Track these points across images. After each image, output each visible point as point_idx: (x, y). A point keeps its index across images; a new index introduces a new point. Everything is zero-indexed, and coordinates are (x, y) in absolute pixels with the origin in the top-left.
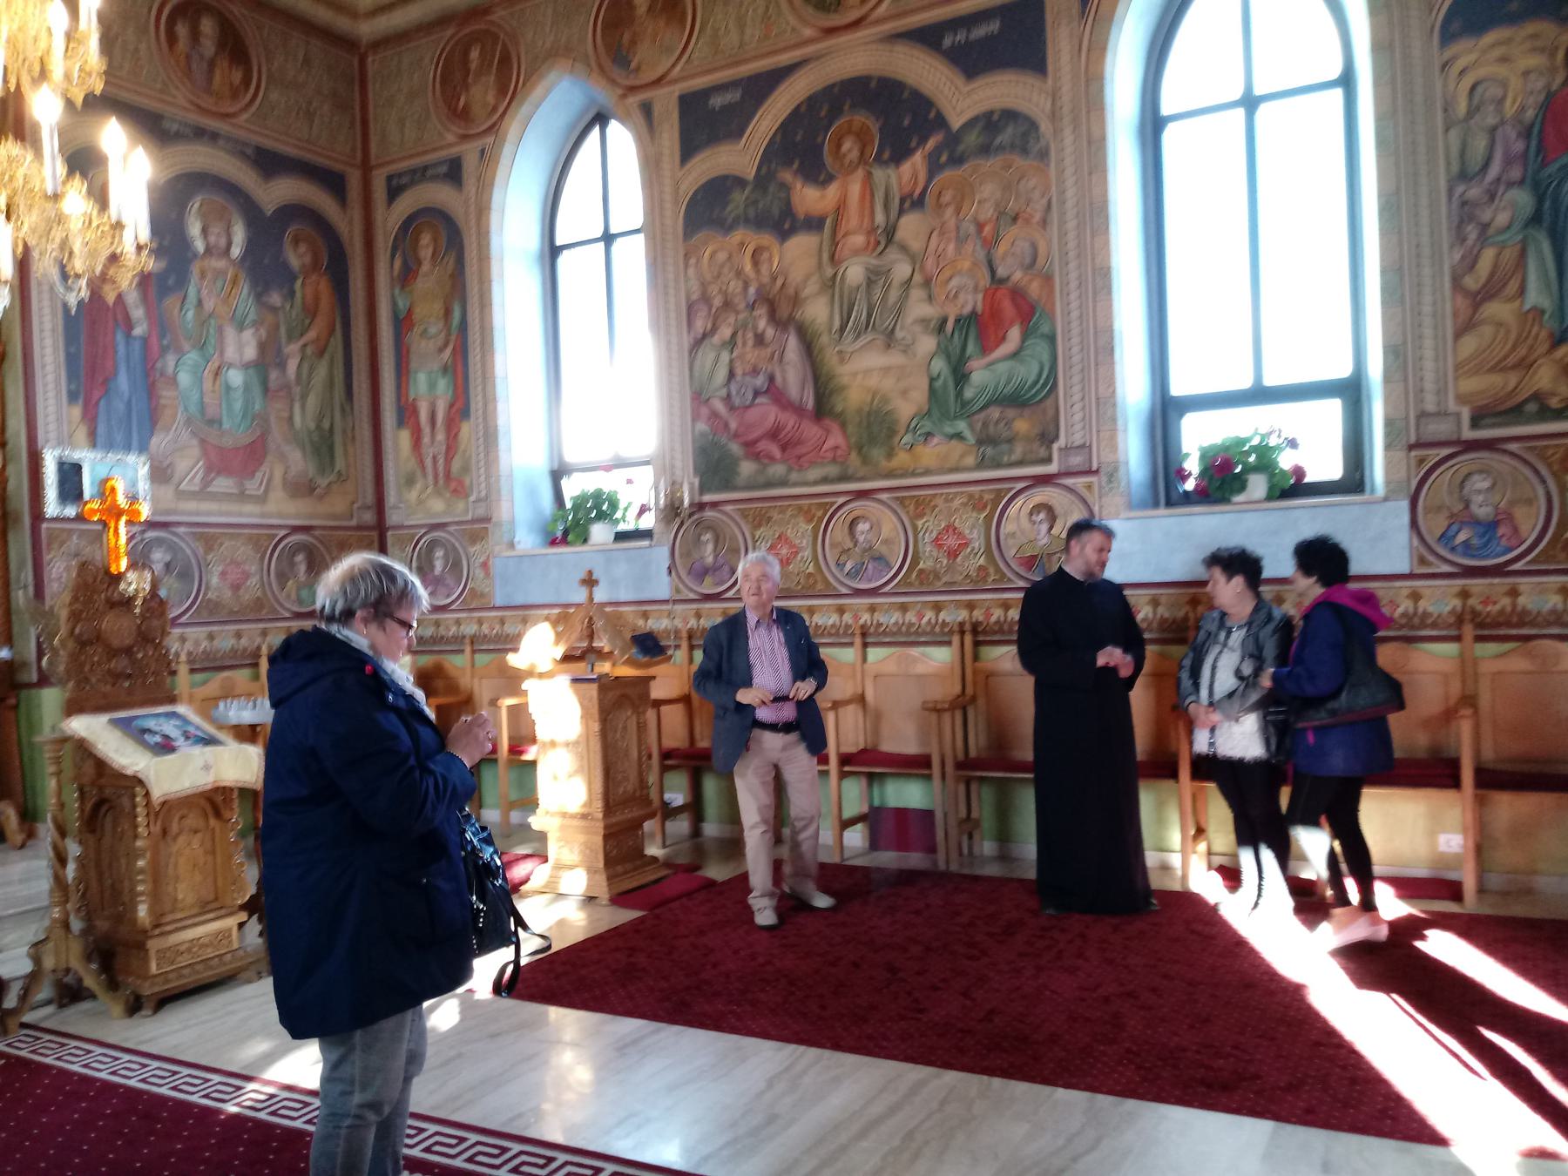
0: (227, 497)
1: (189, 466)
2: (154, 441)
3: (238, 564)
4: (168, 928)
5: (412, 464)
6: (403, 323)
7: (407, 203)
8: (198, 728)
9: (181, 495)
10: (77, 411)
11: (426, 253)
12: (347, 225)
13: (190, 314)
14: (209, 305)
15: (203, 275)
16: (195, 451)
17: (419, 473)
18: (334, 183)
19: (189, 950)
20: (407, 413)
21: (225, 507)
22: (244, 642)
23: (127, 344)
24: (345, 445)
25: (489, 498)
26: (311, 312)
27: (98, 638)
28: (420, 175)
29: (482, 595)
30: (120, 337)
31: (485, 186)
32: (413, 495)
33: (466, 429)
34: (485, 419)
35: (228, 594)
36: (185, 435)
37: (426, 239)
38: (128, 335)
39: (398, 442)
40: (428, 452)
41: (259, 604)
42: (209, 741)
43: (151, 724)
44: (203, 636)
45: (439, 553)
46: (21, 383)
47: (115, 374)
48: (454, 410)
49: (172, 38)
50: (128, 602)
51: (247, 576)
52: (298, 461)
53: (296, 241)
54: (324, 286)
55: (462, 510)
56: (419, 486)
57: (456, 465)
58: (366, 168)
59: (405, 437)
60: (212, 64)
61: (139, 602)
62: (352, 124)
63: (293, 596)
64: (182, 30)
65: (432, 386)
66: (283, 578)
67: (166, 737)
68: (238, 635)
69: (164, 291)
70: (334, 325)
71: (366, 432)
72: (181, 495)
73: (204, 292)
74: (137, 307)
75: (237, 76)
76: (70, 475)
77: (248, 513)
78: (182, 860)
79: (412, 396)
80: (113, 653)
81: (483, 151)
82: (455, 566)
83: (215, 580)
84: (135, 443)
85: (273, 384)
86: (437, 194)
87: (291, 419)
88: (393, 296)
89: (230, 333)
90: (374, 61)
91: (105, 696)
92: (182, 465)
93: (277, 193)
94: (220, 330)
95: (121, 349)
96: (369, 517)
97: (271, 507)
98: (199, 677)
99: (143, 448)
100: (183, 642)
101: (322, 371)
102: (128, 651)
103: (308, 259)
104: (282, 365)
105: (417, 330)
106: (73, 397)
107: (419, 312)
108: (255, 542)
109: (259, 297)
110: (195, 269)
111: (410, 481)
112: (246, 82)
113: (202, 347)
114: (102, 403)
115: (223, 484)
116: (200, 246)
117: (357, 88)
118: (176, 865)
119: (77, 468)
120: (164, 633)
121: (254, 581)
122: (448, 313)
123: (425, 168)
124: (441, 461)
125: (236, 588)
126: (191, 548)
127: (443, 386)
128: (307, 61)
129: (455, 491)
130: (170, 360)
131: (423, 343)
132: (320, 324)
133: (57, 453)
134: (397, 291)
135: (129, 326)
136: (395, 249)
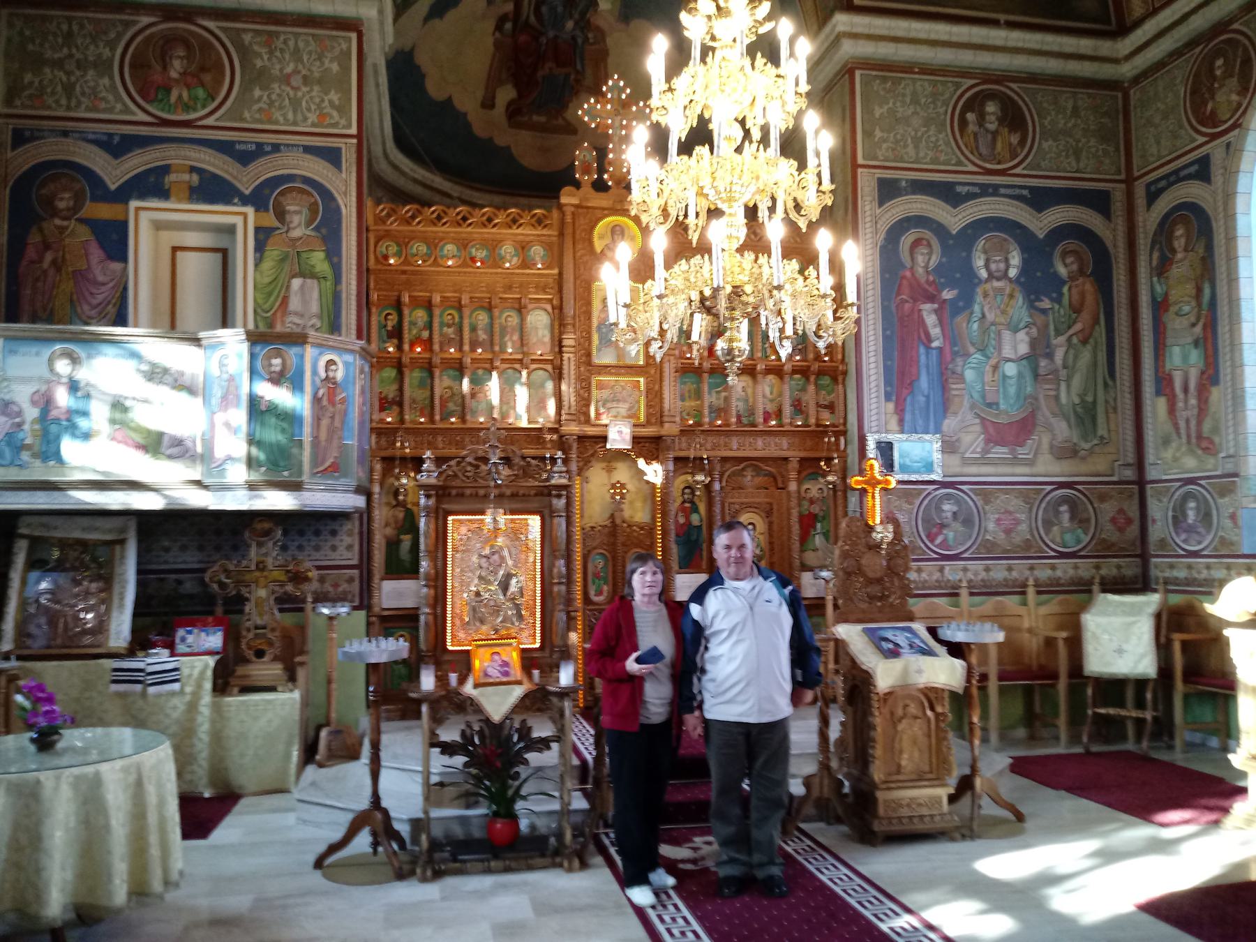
0: (1002, 462)
1: (973, 441)
2: (946, 422)
3: (1010, 513)
4: (893, 785)
5: (1168, 427)
6: (1160, 306)
7: (1164, 204)
8: (923, 641)
10: (891, 406)
11: (1179, 244)
12: (1110, 232)
13: (975, 326)
14: (990, 316)
15: (986, 295)
16: (978, 428)
17: (1174, 436)
18: (1099, 202)
19: (908, 805)
20: (1164, 384)
22: (1015, 574)
23: (927, 354)
24: (1107, 412)
25: (1236, 456)
26: (1077, 309)
27: (860, 571)
28: (1175, 178)
29: (1232, 544)
30: (922, 350)
31: (1231, 174)
32: (1168, 454)
33: (1215, 393)
34: (1234, 385)
35: (1002, 536)
36: (970, 418)
37: (1179, 232)
38: (928, 348)
39: (1156, 408)
40: (1182, 415)
41: (1028, 545)
42: (928, 652)
43: (889, 635)
44: (981, 567)
45: (1192, 504)
47: (918, 378)
49: (963, 123)
50: (876, 547)
51: (1018, 522)
52: (1063, 430)
53: (1064, 254)
55: (1213, 466)
56: (1174, 445)
57: (1207, 427)
58: (1130, 181)
59: (1162, 403)
60: (995, 134)
61: (884, 546)
62: (1117, 150)
63: (1058, 539)
64: (970, 116)
65: (1185, 358)
66: (1048, 524)
67: (897, 645)
68: (1010, 569)
71: (1127, 400)
72: (966, 462)
73: (986, 310)
74: (935, 326)
75: (1015, 139)
76: (886, 450)
77: (1020, 473)
78: (905, 737)
79: (1168, 366)
80: (870, 582)
81: (1228, 145)
82: (1206, 517)
83: (991, 526)
84: (932, 426)
85: (1042, 371)
86: (1191, 191)
87: (1057, 398)
89: (1007, 335)
91: (864, 611)
92: (967, 439)
93: (1041, 223)
94: (999, 334)
95: (923, 358)
96: (1129, 474)
97: (1040, 468)
98: (977, 599)
99: (938, 430)
100: (920, 573)
101: (1086, 355)
102: (879, 581)
103: (1075, 267)
104: (1050, 356)
105: (1173, 309)
106: (888, 398)
107: (1174, 295)
108: (1027, 498)
109: (1031, 306)
110: (979, 290)
111: (1166, 442)
112: (1022, 142)
113: (982, 350)
114: (909, 399)
115: (1000, 452)
116: (984, 274)
117: (1121, 117)
118: (901, 740)
119: (890, 446)
120: (907, 569)
121: (1023, 527)
122: (1199, 290)
123: (1176, 172)
124: (1193, 423)
125: (1008, 532)
126: (971, 501)
127: (1195, 356)
128: (1075, 110)
129: (1206, 450)
131: (1178, 320)
132: (1086, 316)
133: (876, 436)
134: (1155, 279)
135: (929, 339)
136: (1154, 243)
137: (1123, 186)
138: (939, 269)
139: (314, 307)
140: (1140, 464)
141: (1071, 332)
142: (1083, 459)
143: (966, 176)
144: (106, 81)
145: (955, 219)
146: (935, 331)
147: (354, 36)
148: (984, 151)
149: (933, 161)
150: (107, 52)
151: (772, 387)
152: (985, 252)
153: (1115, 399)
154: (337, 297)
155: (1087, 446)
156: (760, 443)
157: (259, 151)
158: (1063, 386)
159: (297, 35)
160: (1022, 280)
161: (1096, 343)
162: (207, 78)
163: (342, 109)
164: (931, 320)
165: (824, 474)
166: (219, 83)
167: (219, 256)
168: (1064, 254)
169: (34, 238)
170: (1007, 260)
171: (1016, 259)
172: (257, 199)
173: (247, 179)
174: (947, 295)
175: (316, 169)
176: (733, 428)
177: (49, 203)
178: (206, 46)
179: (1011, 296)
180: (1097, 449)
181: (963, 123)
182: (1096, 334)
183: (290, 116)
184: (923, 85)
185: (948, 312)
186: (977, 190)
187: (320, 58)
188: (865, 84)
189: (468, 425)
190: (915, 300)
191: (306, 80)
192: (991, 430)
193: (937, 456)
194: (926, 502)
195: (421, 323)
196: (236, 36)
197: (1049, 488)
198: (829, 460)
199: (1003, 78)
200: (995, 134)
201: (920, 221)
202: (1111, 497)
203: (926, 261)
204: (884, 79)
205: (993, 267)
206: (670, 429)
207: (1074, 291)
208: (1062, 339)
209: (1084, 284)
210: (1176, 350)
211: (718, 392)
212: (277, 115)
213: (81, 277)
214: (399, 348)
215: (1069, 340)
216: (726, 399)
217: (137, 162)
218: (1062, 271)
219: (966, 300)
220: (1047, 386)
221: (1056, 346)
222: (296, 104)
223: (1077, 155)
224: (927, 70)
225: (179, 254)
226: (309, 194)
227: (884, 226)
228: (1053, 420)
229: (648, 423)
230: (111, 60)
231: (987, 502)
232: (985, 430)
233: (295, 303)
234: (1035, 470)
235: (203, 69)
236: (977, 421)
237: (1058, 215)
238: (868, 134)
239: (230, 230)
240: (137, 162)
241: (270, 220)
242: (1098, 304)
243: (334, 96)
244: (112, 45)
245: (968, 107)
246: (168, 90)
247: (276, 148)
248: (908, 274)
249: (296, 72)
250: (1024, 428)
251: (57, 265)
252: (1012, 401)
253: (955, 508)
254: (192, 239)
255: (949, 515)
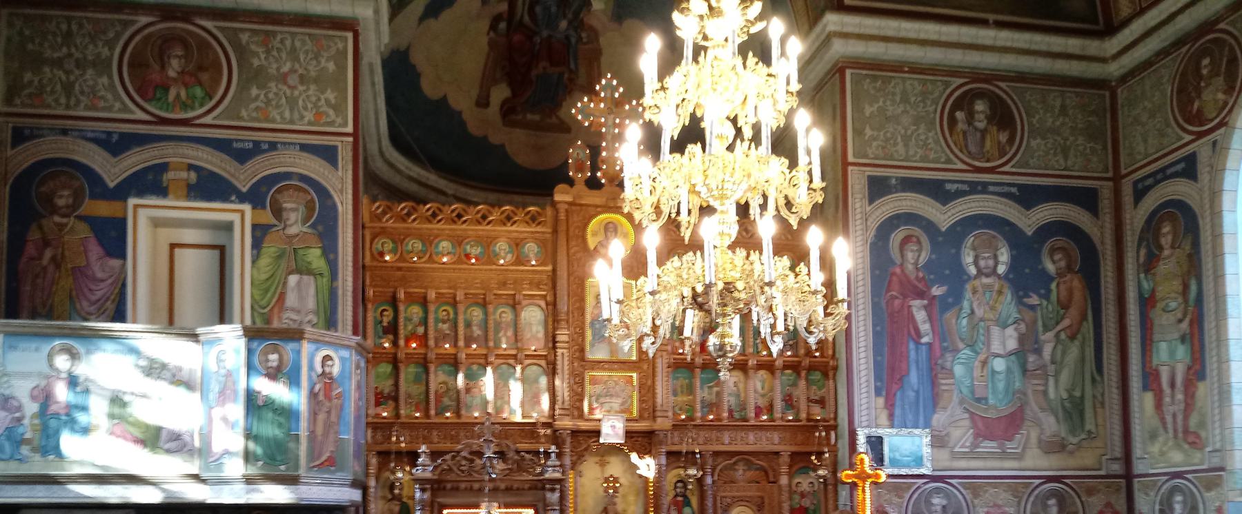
1: (962, 435)
2: (936, 417)
3: (999, 506)
5: (1156, 422)
6: (1147, 302)
7: (1151, 201)
9: (955, 456)
10: (881, 401)
11: (1166, 241)
12: (1098, 229)
13: (964, 322)
14: (979, 313)
15: (975, 292)
16: (967, 423)
17: (1161, 430)
18: (1087, 199)
20: (1151, 379)
21: (990, 464)
23: (917, 350)
25: (1223, 450)
26: (1065, 305)
28: (1162, 176)
30: (912, 346)
31: (1217, 172)
32: (1155, 448)
33: (1202, 389)
34: (1220, 380)
36: (959, 411)
37: (1166, 229)
38: (918, 343)
39: (1143, 403)
40: (1169, 410)
45: (1179, 498)
46: (845, 386)
47: (908, 373)
48: (1192, 372)
49: (953, 122)
52: (1051, 425)
53: (1052, 251)
54: (1077, 283)
55: (1199, 460)
56: (1161, 439)
57: (1193, 421)
58: (1117, 179)
59: (1149, 398)
60: (984, 132)
62: (1105, 148)
64: (959, 115)
65: (1172, 353)
69: (946, 307)
70: (1086, 310)
71: (1114, 395)
72: (955, 456)
73: (975, 306)
75: (1003, 137)
76: (876, 444)
77: (1009, 467)
79: (1155, 362)
81: (1215, 143)
85: (1030, 367)
86: (1178, 189)
87: (1045, 393)
88: (1139, 282)
89: (995, 331)
90: (1122, 92)
92: (956, 433)
93: (1029, 220)
94: (988, 330)
95: (912, 354)
96: (1117, 468)
97: (1028, 462)
101: (1074, 351)
103: (1063, 264)
104: (1038, 351)
105: (1160, 305)
106: (878, 393)
107: (1161, 291)
108: (1015, 492)
109: (1020, 302)
110: (968, 287)
111: (1153, 436)
112: (1011, 140)
113: (971, 346)
114: (898, 394)
115: (989, 446)
116: (973, 270)
117: (1108, 115)
119: (880, 440)
122: (1186, 287)
123: (1163, 170)
124: (1180, 418)
127: (1182, 352)
129: (1192, 444)
130: (949, 356)
131: (1165, 316)
132: (1074, 312)
133: (866, 431)
134: (1142, 276)
135: (919, 335)
136: (1141, 240)
137: (1111, 184)
138: (928, 266)
139: (311, 303)
140: (1127, 458)
141: (1059, 328)
142: (1071, 453)
143: (955, 174)
144: (105, 80)
145: (944, 216)
146: (925, 327)
147: (350, 35)
148: (973, 149)
149: (923, 159)
150: (105, 52)
151: (763, 382)
152: (974, 248)
153: (1103, 395)
154: (333, 293)
155: (1075, 440)
156: (751, 437)
157: (257, 149)
158: (1051, 382)
159: (293, 35)
160: (1011, 276)
161: (1084, 338)
162: (205, 77)
163: (339, 108)
164: (920, 316)
165: (815, 468)
166: (217, 81)
167: (216, 253)
168: (1052, 251)
169: (34, 235)
170: (995, 257)
171: (1004, 256)
172: (255, 197)
173: (244, 177)
174: (937, 291)
175: (312, 167)
176: (725, 422)
177: (48, 200)
178: (204, 46)
179: (1000, 292)
180: (1085, 444)
181: (953, 122)
182: (1084, 330)
183: (287, 114)
184: (913, 84)
185: (937, 308)
186: (966, 187)
187: (317, 57)
188: (856, 82)
189: (463, 420)
190: (905, 296)
191: (303, 79)
192: (980, 424)
193: (926, 451)
194: (915, 496)
195: (416, 319)
196: (233, 35)
197: (1038, 482)
198: (820, 454)
199: (992, 77)
200: (984, 132)
201: (910, 218)
202: (1099, 491)
203: (915, 258)
204: (875, 78)
205: (982, 263)
206: (662, 423)
207: (1062, 287)
208: (1050, 335)
209: (1072, 281)
210: (1163, 345)
211: (710, 388)
212: (274, 114)
213: (81, 273)
214: (395, 343)
215: (1057, 335)
216: (718, 394)
217: (135, 160)
218: (1050, 267)
219: (955, 296)
220: (1036, 382)
221: (1045, 342)
222: (292, 103)
223: (1065, 153)
224: (916, 69)
225: (177, 251)
226: (305, 191)
227: (874, 224)
228: (1041, 415)
229: (641, 417)
230: (110, 59)
231: (976, 495)
232: (974, 425)
233: (291, 300)
234: (1023, 464)
235: (201, 68)
236: (967, 416)
237: (1047, 213)
238: (858, 132)
239: (228, 227)
240: (135, 160)
241: (267, 217)
242: (1086, 300)
243: (330, 95)
244: (111, 45)
245: (957, 106)
246: (166, 89)
247: (273, 146)
248: (898, 271)
249: (293, 71)
250: (1013, 422)
251: (57, 262)
252: (1001, 396)
253: (944, 502)
254: (190, 236)
255: (939, 508)
